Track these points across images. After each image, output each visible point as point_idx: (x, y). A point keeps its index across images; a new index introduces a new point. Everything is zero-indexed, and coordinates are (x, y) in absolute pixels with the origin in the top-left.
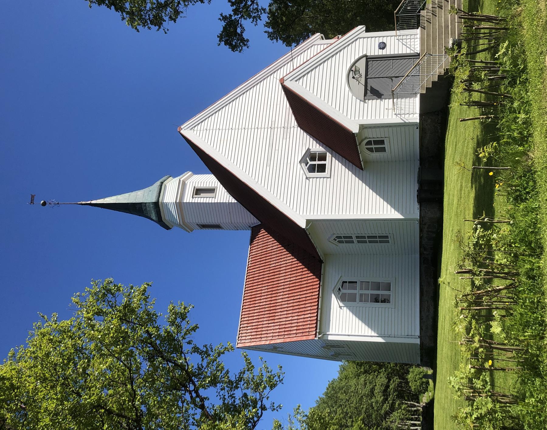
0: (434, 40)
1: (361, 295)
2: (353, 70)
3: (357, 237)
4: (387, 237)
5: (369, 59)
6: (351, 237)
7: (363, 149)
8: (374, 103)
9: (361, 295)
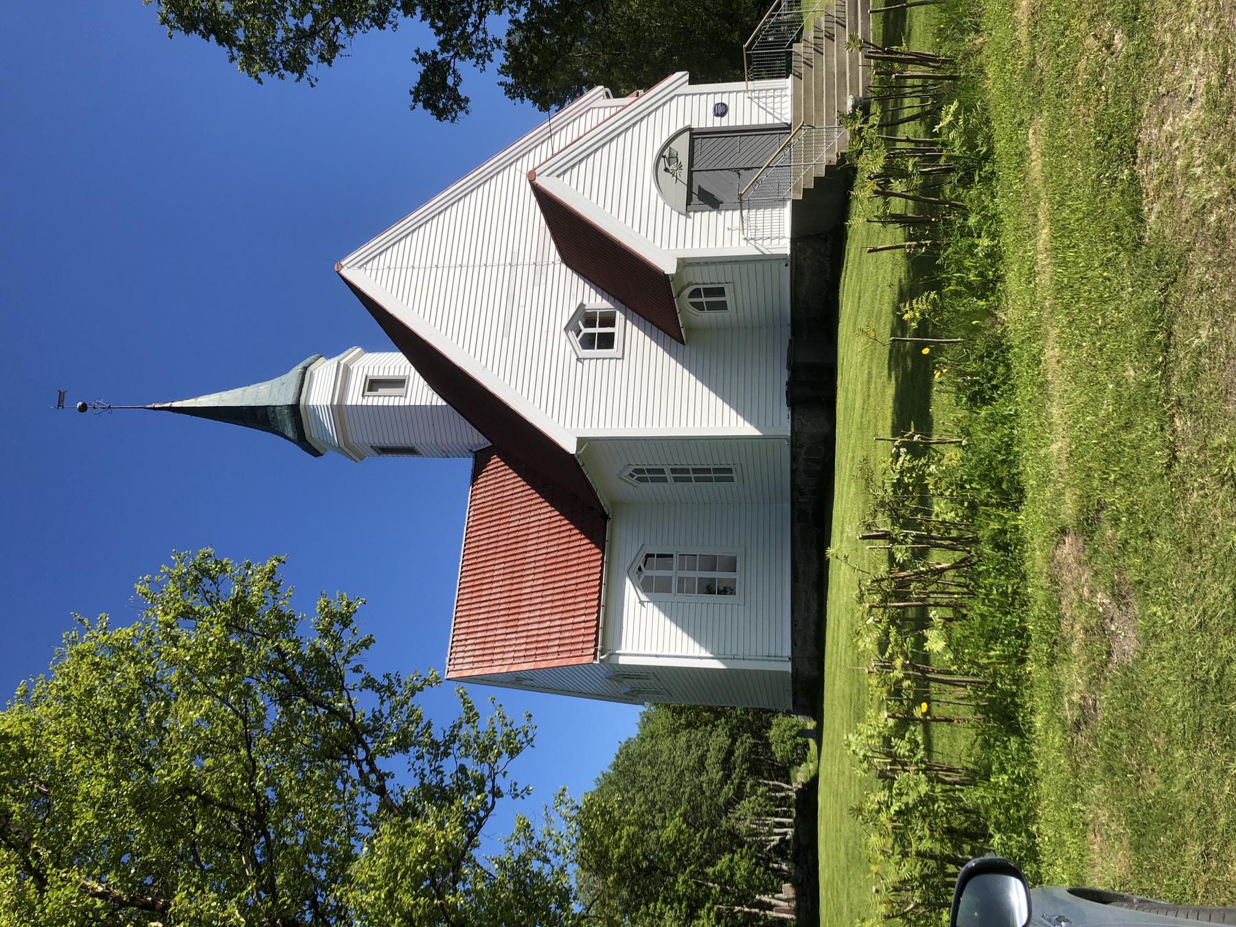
0: (818, 99)
1: (681, 580)
2: (665, 156)
3: (673, 471)
4: (730, 470)
5: (695, 135)
6: (662, 471)
7: (683, 304)
8: (705, 219)
9: (681, 580)
